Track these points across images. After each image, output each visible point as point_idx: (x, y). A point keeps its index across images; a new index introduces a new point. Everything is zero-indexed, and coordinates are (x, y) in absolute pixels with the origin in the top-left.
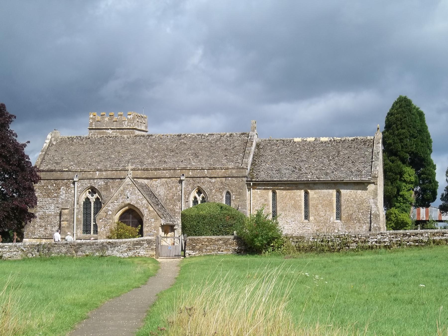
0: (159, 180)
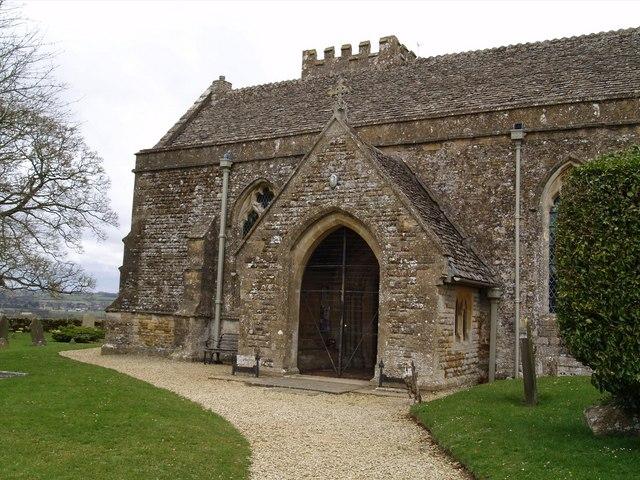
0: (441, 150)
